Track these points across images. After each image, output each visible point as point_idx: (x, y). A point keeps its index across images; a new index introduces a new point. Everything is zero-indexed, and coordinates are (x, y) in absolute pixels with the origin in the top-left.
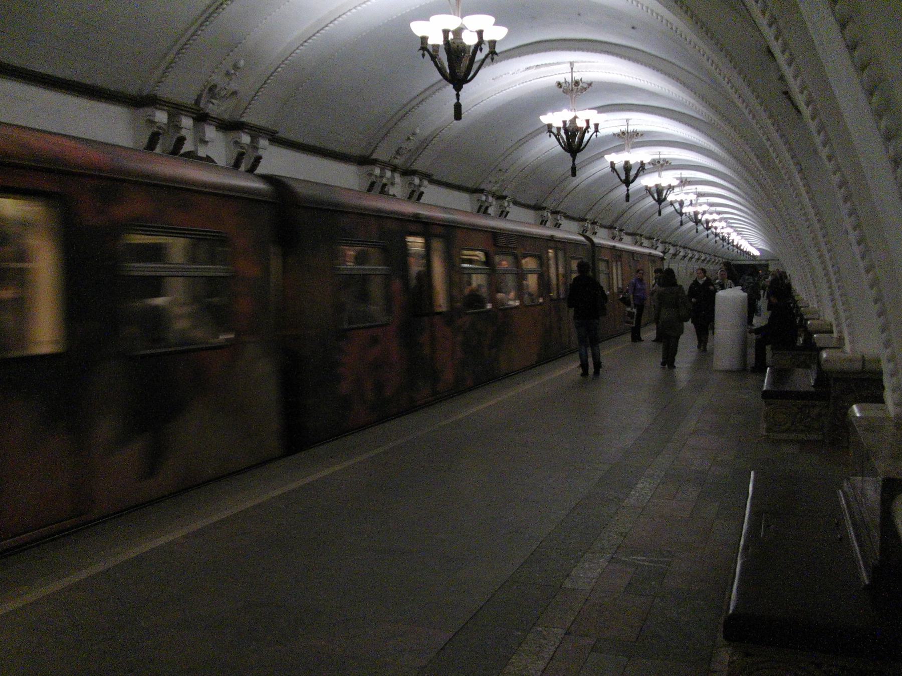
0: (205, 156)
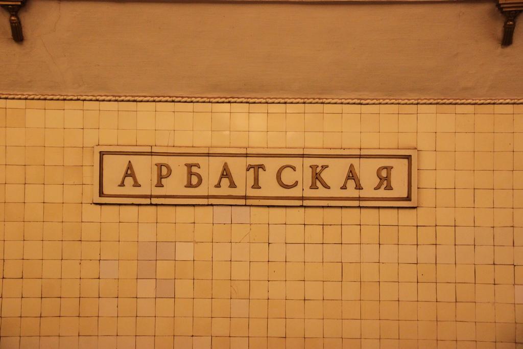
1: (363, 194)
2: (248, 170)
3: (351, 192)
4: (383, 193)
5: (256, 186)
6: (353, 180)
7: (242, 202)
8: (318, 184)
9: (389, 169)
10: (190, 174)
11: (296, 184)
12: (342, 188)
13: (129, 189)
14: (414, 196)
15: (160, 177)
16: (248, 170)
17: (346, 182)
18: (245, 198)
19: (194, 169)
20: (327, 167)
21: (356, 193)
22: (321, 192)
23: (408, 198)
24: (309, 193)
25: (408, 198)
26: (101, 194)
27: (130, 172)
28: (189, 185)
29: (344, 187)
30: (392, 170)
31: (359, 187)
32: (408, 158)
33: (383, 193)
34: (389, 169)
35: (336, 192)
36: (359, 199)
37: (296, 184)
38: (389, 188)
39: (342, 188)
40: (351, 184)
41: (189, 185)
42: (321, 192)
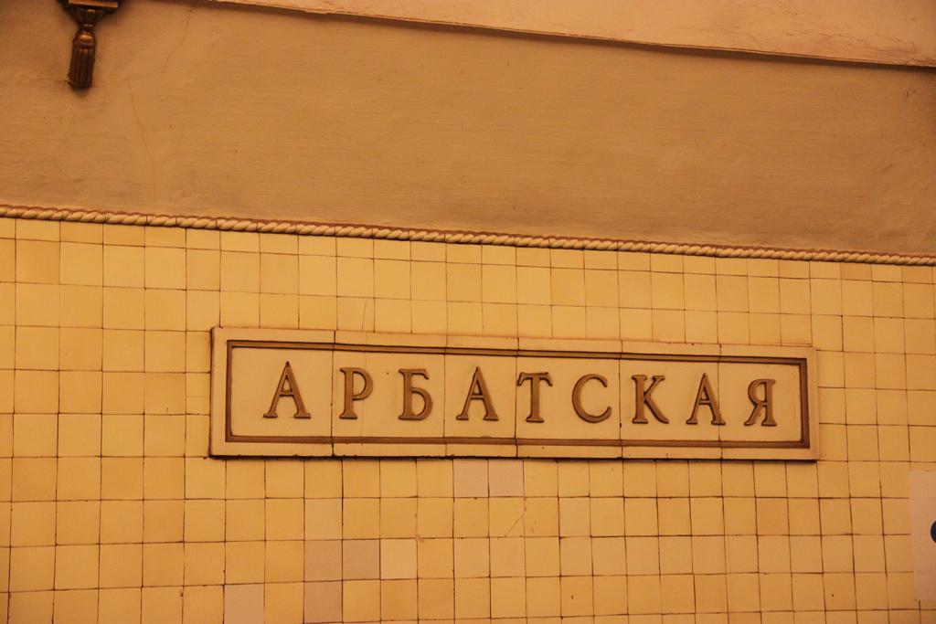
1: (726, 434)
2: (519, 384)
3: (705, 431)
4: (758, 433)
5: (534, 418)
6: (291, 399)
7: (509, 450)
8: (648, 414)
10: (410, 391)
11: (607, 414)
12: (688, 423)
13: (286, 424)
14: (813, 438)
15: (351, 398)
16: (519, 384)
18: (515, 441)
19: (418, 382)
21: (712, 433)
22: (653, 430)
23: (804, 443)
24: (632, 432)
27: (288, 387)
28: (407, 416)
29: (271, 415)
30: (774, 386)
31: (717, 421)
32: (799, 365)
33: (758, 433)
35: (678, 431)
36: (720, 444)
37: (607, 414)
38: (769, 422)
39: (688, 423)
40: (704, 413)
42: (653, 430)
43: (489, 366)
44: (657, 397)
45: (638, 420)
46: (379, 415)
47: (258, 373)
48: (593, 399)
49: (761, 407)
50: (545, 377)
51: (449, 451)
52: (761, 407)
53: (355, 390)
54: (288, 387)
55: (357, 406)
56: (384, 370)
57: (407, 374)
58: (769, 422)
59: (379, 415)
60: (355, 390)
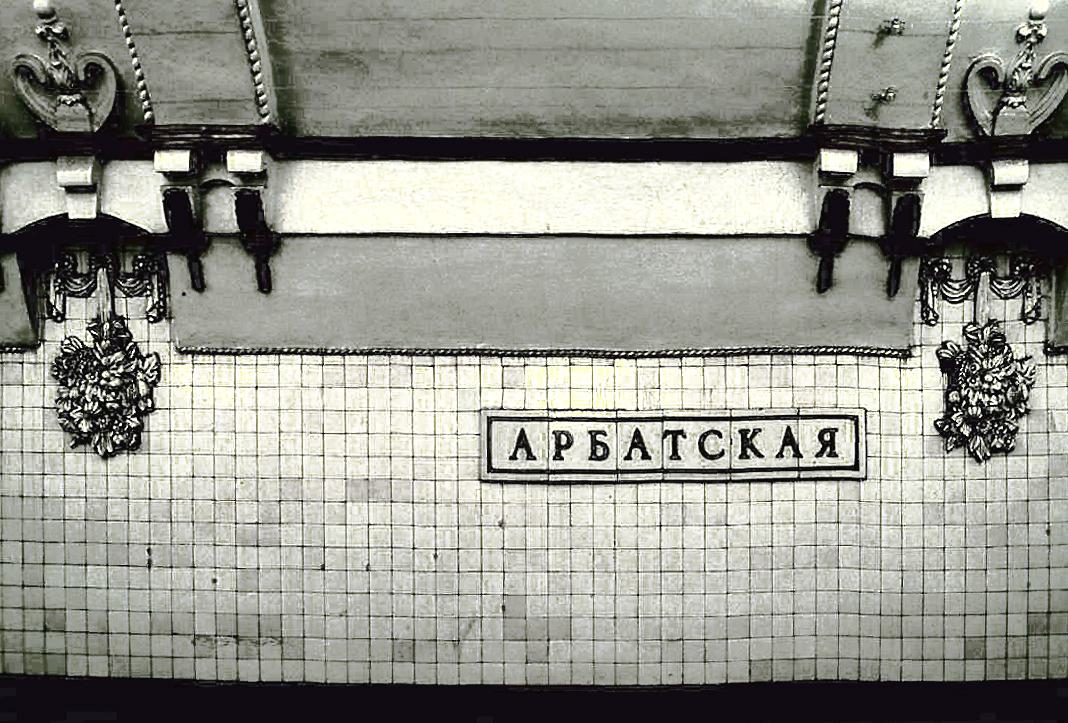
0: (1017, 216)
2: (664, 436)
3: (789, 460)
4: (826, 461)
5: (675, 456)
8: (749, 451)
9: (833, 432)
10: (595, 443)
11: (722, 454)
14: (862, 468)
15: (559, 447)
16: (664, 436)
17: (782, 449)
18: (664, 471)
19: (599, 438)
20: (760, 430)
23: (856, 467)
25: (856, 467)
26: (490, 469)
27: (522, 442)
33: (826, 461)
34: (833, 432)
36: (799, 469)
37: (722, 454)
38: (833, 454)
41: (594, 457)
43: (528, 427)
44: (758, 442)
45: (744, 456)
46: (577, 457)
47: (505, 436)
48: (711, 445)
49: (828, 444)
50: (681, 432)
51: (618, 477)
52: (828, 444)
53: (563, 443)
54: (522, 442)
55: (563, 453)
56: (580, 432)
57: (593, 434)
58: (833, 454)
59: (577, 457)
60: (563, 443)
